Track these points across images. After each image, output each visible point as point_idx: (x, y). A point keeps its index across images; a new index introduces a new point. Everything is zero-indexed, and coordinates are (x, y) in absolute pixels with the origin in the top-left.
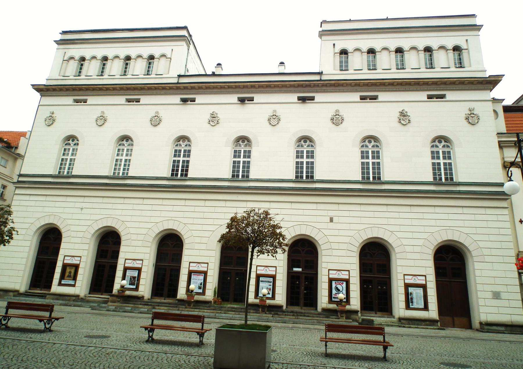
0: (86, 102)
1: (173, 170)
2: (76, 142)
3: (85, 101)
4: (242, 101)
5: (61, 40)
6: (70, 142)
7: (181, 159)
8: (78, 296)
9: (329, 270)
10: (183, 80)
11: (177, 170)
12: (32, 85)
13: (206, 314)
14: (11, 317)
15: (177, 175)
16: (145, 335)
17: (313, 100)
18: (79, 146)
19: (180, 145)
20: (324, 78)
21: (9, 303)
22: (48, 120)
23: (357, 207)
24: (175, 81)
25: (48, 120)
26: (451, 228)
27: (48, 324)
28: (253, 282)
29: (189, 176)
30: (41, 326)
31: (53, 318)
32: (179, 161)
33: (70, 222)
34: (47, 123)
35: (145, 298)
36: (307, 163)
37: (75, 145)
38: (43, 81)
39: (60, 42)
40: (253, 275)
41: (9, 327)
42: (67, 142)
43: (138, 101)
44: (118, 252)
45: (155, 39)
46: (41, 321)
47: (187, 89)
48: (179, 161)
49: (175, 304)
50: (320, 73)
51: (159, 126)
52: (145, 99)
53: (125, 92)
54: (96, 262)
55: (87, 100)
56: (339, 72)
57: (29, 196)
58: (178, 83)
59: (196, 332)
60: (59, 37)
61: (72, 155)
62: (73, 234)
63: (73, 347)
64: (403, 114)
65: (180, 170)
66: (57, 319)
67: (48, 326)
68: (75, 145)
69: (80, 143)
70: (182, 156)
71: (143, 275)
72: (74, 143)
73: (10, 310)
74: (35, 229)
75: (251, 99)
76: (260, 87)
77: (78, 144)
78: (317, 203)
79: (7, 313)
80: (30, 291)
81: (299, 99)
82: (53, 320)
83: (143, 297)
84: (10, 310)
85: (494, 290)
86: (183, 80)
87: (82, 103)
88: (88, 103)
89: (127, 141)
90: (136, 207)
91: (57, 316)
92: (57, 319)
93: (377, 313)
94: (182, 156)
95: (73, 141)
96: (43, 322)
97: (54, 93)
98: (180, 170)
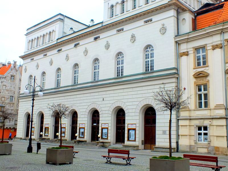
0: (152, 21)
1: (146, 68)
2: (151, 48)
3: (151, 20)
4: (96, 39)
5: (27, 33)
6: (148, 49)
7: (150, 59)
8: (22, 138)
9: (128, 124)
10: (59, 41)
11: (148, 67)
12: (19, 57)
13: (130, 149)
14: (111, 157)
15: (148, 70)
16: (105, 160)
17: (123, 30)
18: (154, 51)
19: (148, 51)
20: (104, 24)
21: (109, 150)
22: (162, 30)
23: (112, 92)
24: (56, 42)
25: (162, 30)
26: (119, 100)
27: (128, 161)
28: (126, 132)
29: (154, 70)
30: (124, 162)
31: (130, 158)
32: (148, 61)
33: (101, 106)
34: (161, 32)
35: (87, 142)
36: (151, 60)
37: (151, 50)
38: (23, 54)
39: (27, 34)
40: (78, 128)
41: (111, 162)
42: (118, 57)
43: (151, 20)
44: (124, 120)
45: (35, 31)
46: (124, 159)
47: (75, 39)
48: (148, 61)
49: (96, 144)
50: (102, 23)
51: (165, 34)
52: (126, 27)
53: (151, 14)
54: (145, 127)
55: (152, 19)
56: (109, 19)
57: (105, 92)
58: (102, 26)
59: (211, 168)
60: (26, 32)
61: (151, 57)
62: (104, 112)
63: (108, 169)
64: (133, 36)
65: (120, 73)
66: (133, 158)
67: (128, 162)
68: (151, 50)
69: (154, 48)
70: (150, 57)
71: (109, 132)
72: (151, 49)
73: (110, 153)
74: (88, 111)
75: (78, 44)
76: (80, 37)
77: (153, 50)
78: (48, 98)
79: (109, 155)
80: (26, 138)
81: (146, 22)
82: (130, 159)
83: (66, 140)
84: (110, 153)
85: (164, 130)
86: (59, 41)
87: (150, 22)
88: (124, 30)
89: (150, 48)
90: (120, 94)
91: (132, 157)
92: (133, 158)
93: (122, 143)
94: (150, 57)
95: (150, 48)
96: (125, 160)
97: (134, 20)
98: (149, 68)
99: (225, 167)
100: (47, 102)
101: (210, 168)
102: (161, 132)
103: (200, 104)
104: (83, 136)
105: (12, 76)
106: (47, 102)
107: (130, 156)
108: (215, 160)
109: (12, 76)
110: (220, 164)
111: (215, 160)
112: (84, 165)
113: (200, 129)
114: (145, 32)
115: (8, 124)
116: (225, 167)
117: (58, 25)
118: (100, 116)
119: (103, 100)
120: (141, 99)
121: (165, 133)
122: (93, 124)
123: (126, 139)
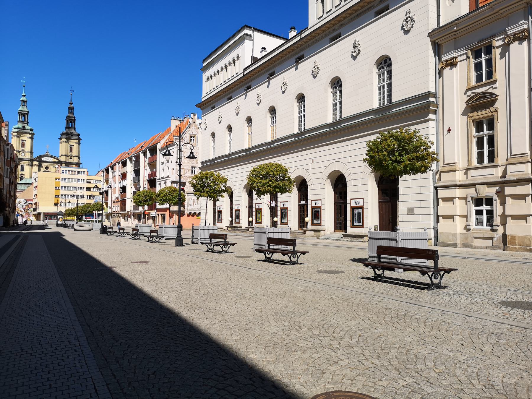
27: (435, 278)
28: (349, 212)
59: (419, 271)
99: (457, 270)
100: (311, 156)
101: (418, 272)
102: (405, 211)
103: (480, 156)
104: (361, 224)
105: (191, 137)
106: (311, 156)
107: (440, 264)
108: (433, 255)
109: (191, 137)
110: (442, 263)
111: (433, 255)
112: (354, 293)
113: (478, 202)
114: (20, 182)
115: (192, 207)
116: (457, 270)
117: (204, 94)
118: (309, 188)
119: (313, 162)
120: (327, 164)
121: (413, 212)
122: (299, 202)
123: (349, 224)
